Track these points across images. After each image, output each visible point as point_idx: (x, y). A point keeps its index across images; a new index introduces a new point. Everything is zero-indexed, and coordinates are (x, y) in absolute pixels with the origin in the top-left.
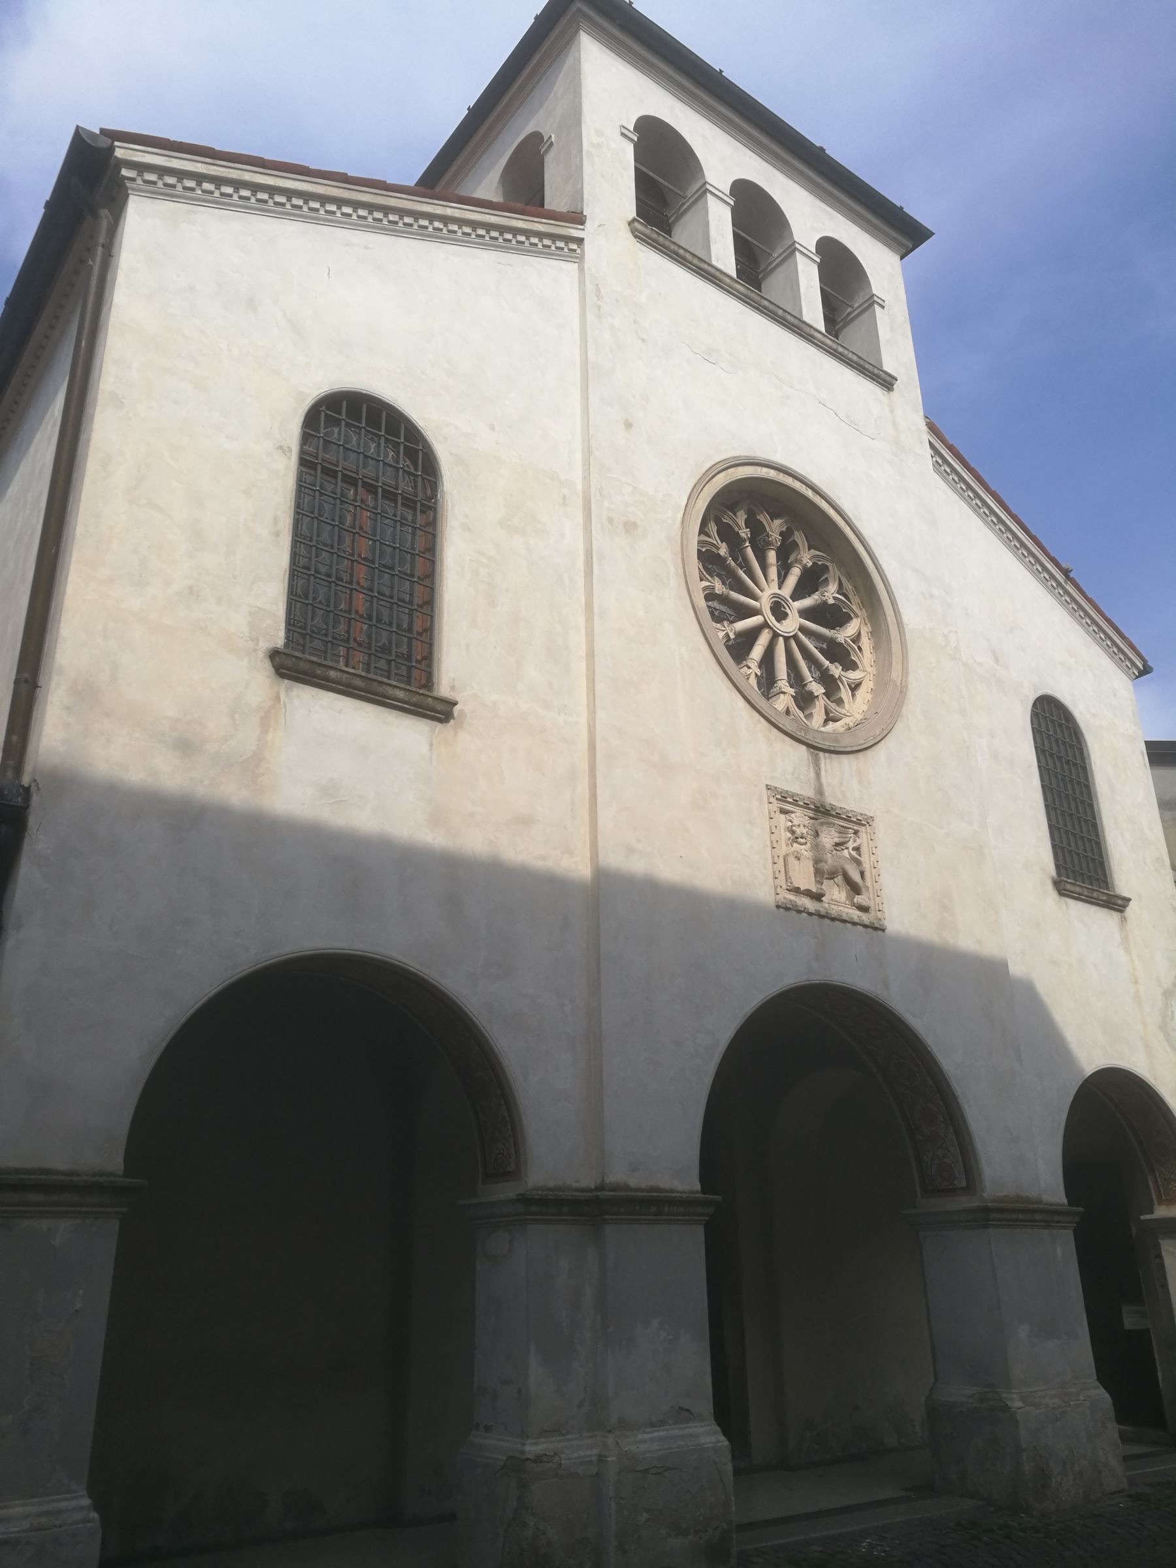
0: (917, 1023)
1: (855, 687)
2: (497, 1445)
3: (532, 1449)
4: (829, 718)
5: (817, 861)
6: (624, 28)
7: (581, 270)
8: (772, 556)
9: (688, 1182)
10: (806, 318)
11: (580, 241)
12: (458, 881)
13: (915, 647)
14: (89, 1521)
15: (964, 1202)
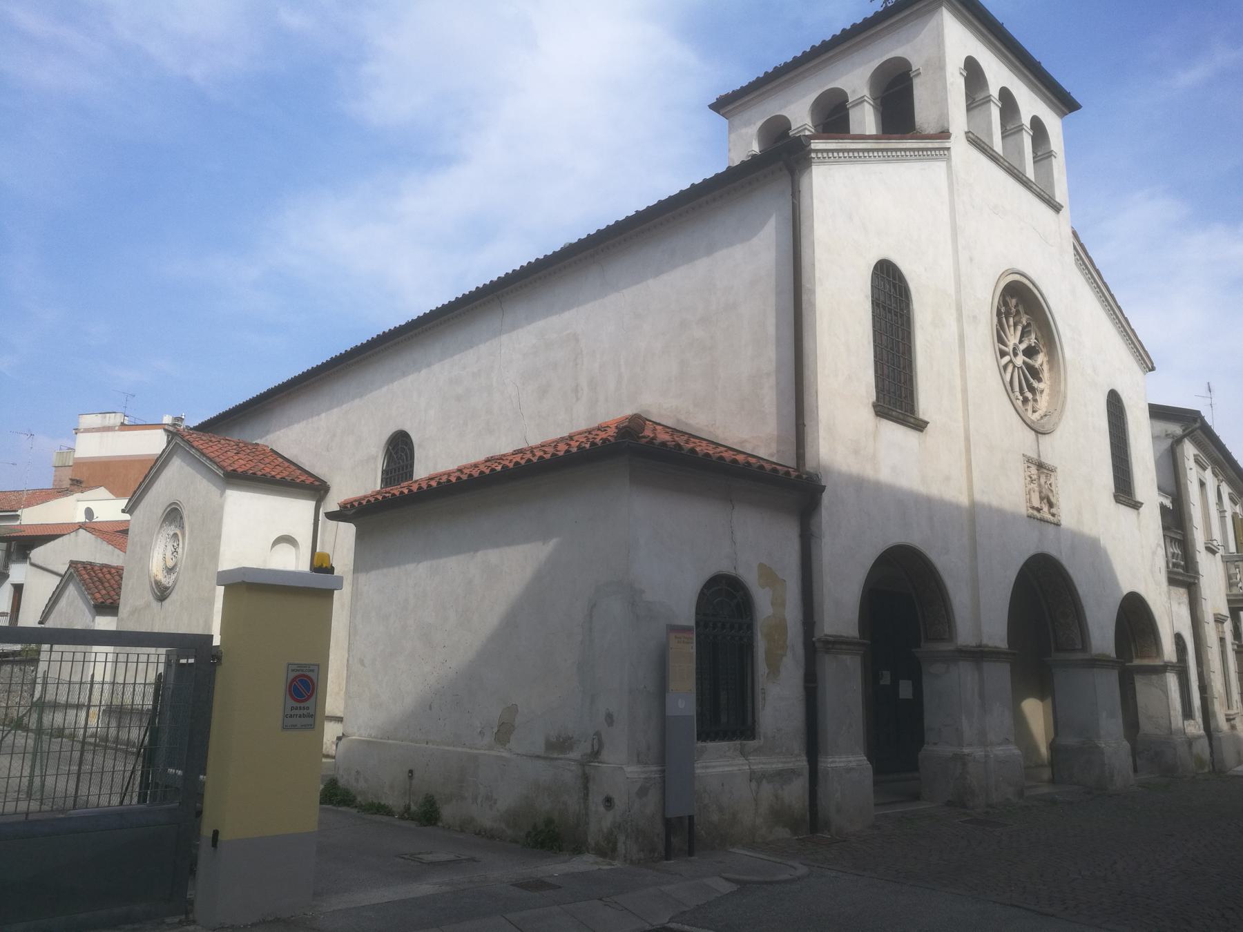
0: (1071, 571)
1: (1042, 392)
3: (966, 750)
4: (1034, 412)
5: (1040, 492)
7: (949, 168)
8: (1020, 328)
9: (692, 623)
10: (1057, 200)
11: (948, 149)
12: (928, 506)
13: (1069, 368)
15: (1080, 656)
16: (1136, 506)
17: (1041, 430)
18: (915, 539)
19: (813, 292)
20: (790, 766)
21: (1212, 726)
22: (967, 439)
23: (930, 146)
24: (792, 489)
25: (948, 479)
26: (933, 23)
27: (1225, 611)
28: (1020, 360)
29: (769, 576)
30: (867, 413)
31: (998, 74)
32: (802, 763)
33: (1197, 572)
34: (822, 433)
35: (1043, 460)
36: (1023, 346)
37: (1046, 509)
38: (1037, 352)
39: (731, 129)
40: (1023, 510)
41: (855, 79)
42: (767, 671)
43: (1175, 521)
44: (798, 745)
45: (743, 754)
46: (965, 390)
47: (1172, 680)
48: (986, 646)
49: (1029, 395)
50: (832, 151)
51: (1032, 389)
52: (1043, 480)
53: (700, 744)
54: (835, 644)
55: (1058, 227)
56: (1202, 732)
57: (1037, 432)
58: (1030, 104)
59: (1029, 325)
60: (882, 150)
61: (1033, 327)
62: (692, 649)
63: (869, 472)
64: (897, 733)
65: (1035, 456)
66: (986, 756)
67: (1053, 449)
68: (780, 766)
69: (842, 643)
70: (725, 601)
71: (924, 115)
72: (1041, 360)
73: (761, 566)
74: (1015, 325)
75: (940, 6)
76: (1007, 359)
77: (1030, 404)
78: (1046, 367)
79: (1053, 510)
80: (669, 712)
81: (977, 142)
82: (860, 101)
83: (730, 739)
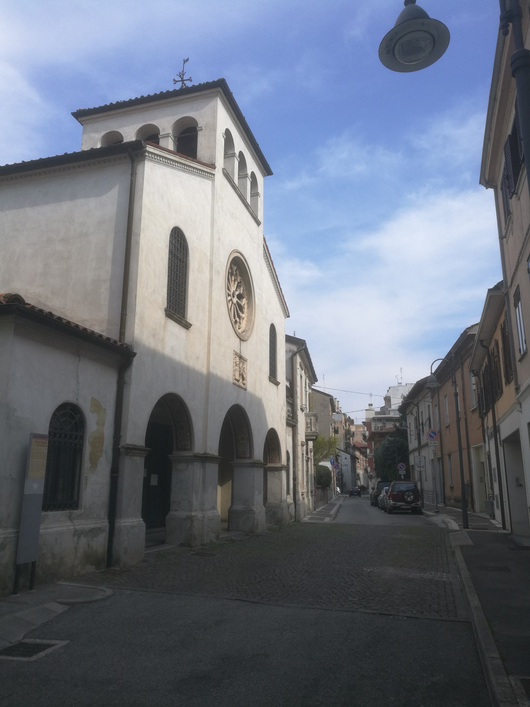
1: (243, 319)
2: (119, 524)
3: (194, 514)
4: (239, 329)
5: (240, 371)
6: (228, 99)
7: (213, 185)
8: (236, 283)
9: (47, 433)
14: (44, 529)
16: (277, 384)
17: (242, 339)
18: (179, 391)
19: (139, 235)
20: (99, 525)
21: (297, 498)
22: (209, 338)
23: (205, 170)
24: (116, 354)
25: (198, 358)
26: (212, 104)
27: (304, 441)
28: (235, 300)
29: (97, 406)
30: (161, 314)
31: (240, 145)
32: (106, 523)
33: (297, 420)
34: (137, 321)
35: (242, 355)
36: (237, 293)
37: (241, 381)
38: (243, 298)
39: (84, 132)
40: (231, 380)
41: (165, 122)
42: (90, 466)
43: (291, 393)
44: (103, 513)
45: (71, 519)
46: (210, 311)
47: (284, 473)
48: (209, 454)
49: (238, 319)
50: (158, 155)
51: (239, 317)
52: (241, 365)
53: (43, 513)
54: (132, 450)
55: (258, 232)
56: (292, 501)
57: (241, 339)
58: (252, 166)
59: (241, 282)
60: (183, 164)
61: (242, 284)
62: (45, 450)
63: (159, 348)
64: (157, 504)
65: (239, 352)
66: (203, 517)
67: (247, 350)
68: (93, 526)
69: (136, 449)
70: (68, 420)
71: (202, 151)
72: (244, 302)
73: (93, 399)
74: (235, 281)
75: (217, 96)
76: (229, 298)
77: (238, 324)
78: (246, 306)
79: (244, 382)
80: (27, 492)
81: (228, 176)
82: (167, 136)
83: (63, 510)
